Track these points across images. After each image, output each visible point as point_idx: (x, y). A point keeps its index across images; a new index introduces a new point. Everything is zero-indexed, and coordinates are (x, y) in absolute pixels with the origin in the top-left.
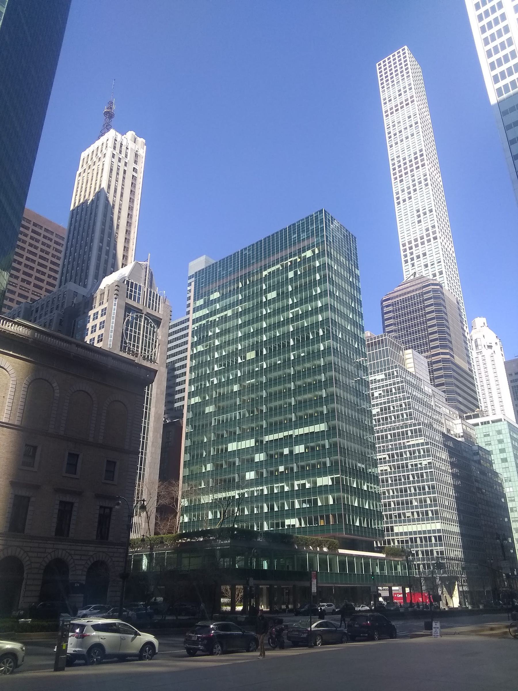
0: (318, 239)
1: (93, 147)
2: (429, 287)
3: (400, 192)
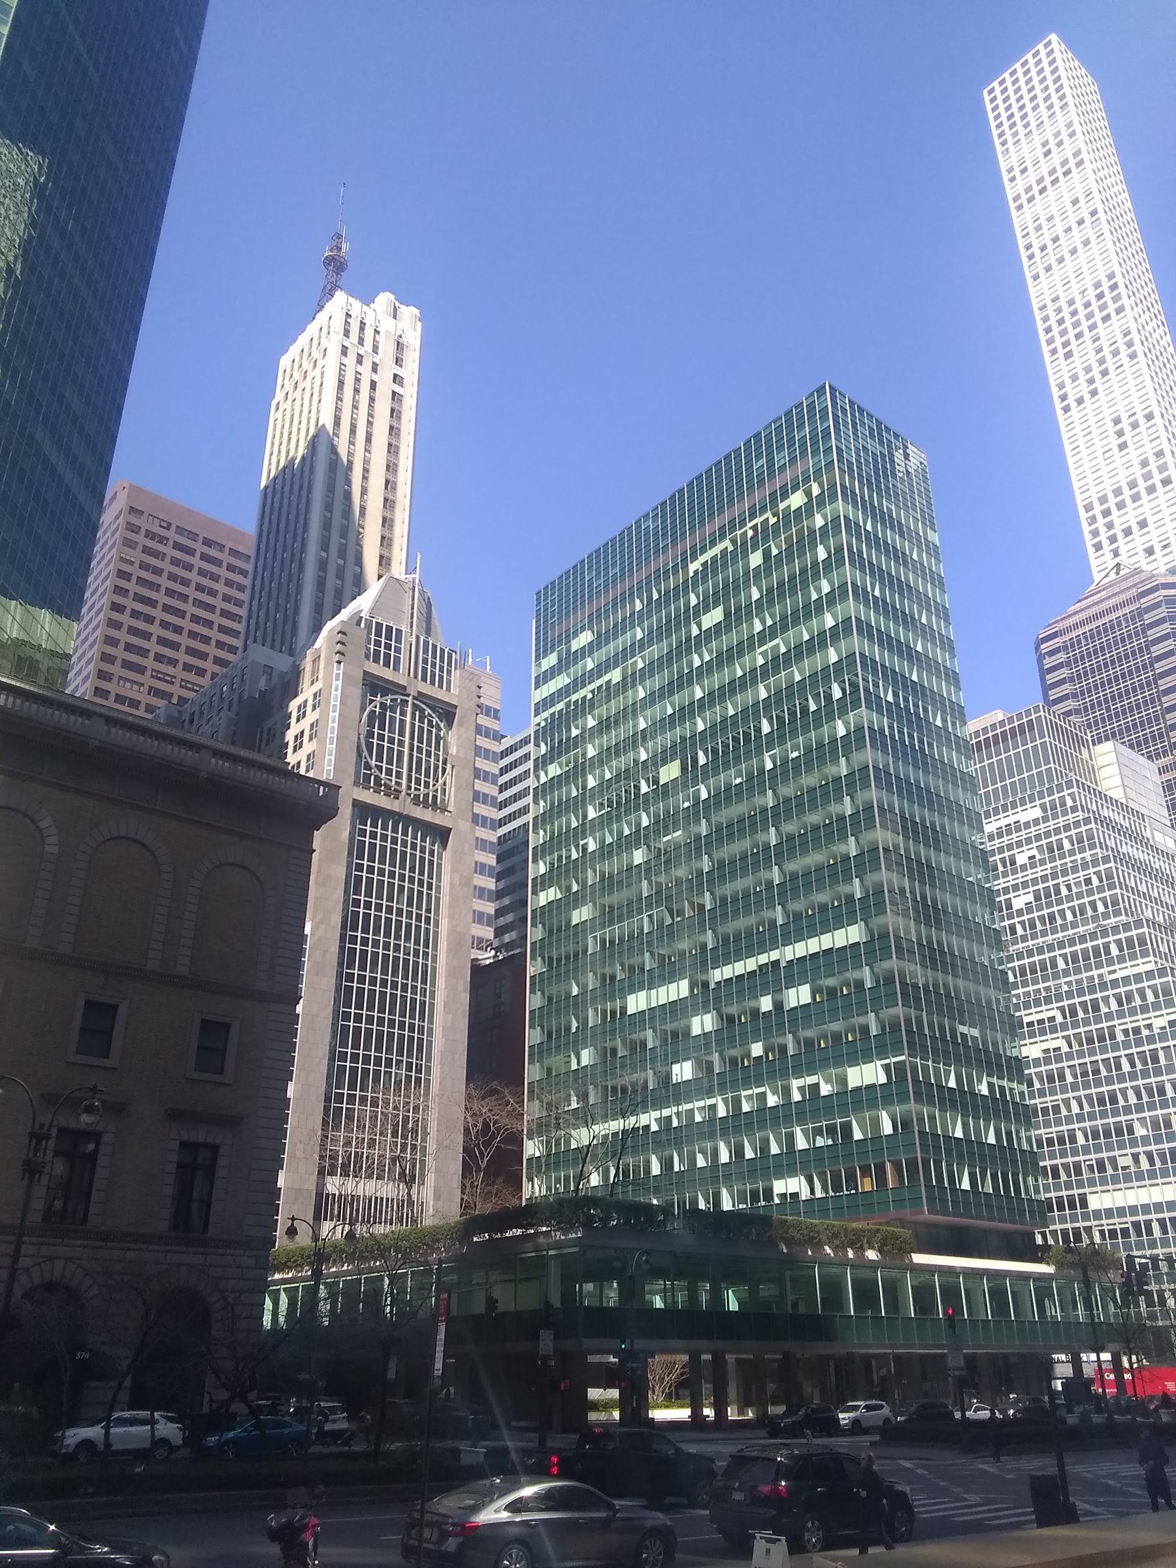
0: (816, 459)
1: (303, 340)
2: (1156, 594)
3: (1068, 382)
